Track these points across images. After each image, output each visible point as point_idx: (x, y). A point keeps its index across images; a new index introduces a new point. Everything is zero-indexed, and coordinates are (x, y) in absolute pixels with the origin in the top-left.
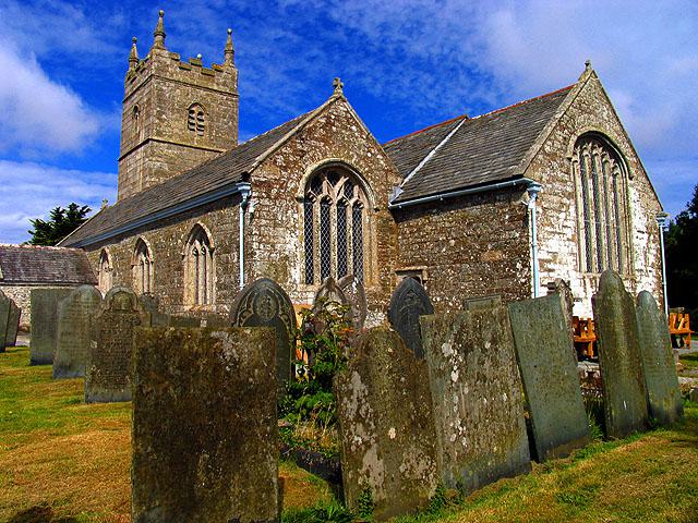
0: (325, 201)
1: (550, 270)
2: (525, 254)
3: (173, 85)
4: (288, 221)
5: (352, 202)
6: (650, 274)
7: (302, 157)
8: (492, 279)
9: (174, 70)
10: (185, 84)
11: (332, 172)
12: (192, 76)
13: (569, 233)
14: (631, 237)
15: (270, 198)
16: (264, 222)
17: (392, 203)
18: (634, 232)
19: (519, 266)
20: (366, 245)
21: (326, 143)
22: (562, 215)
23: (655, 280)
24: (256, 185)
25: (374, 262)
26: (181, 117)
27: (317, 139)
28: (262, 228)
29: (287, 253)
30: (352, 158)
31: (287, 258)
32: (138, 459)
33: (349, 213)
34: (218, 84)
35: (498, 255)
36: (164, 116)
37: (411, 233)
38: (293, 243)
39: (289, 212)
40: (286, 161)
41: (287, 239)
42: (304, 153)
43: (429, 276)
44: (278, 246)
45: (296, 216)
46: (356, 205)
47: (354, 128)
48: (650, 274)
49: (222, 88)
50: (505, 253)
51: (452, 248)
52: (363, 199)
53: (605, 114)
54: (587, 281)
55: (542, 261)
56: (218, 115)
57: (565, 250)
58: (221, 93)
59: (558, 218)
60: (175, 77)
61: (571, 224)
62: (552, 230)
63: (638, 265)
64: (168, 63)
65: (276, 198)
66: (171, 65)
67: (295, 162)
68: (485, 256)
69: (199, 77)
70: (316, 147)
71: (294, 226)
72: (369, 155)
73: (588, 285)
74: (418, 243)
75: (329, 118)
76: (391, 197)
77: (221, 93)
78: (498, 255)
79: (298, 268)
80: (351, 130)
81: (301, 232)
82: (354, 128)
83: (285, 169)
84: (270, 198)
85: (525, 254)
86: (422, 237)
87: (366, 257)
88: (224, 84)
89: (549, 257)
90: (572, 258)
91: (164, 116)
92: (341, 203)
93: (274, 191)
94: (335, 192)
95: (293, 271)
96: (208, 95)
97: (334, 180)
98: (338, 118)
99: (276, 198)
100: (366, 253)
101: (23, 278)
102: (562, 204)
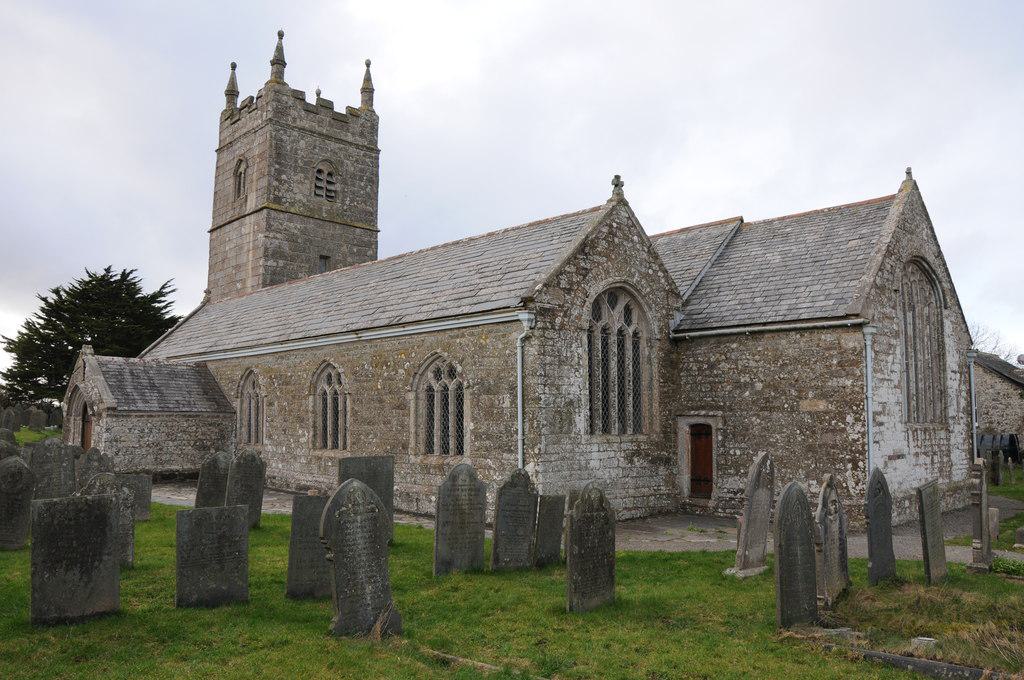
0: (604, 330)
1: (881, 424)
2: (858, 406)
3: (295, 133)
4: (572, 357)
5: (631, 330)
6: (962, 421)
7: (585, 277)
8: (814, 432)
10: (312, 132)
11: (612, 295)
12: (320, 122)
13: (895, 377)
14: (945, 378)
15: (554, 329)
17: (676, 331)
18: (949, 371)
19: (849, 419)
20: (644, 383)
21: (608, 256)
22: (890, 358)
23: (966, 428)
25: (656, 405)
26: (306, 178)
27: (600, 254)
29: (571, 396)
30: (633, 276)
31: (571, 403)
33: (629, 345)
34: (353, 134)
35: (822, 405)
36: (284, 177)
37: (699, 369)
40: (571, 283)
43: (725, 423)
45: (580, 351)
46: (635, 334)
47: (635, 238)
48: (962, 421)
50: (831, 403)
51: (758, 393)
52: (642, 328)
53: (924, 233)
54: (910, 432)
55: (875, 414)
56: (353, 177)
57: (893, 399)
58: (357, 146)
59: (887, 362)
60: (299, 123)
61: (897, 367)
62: (882, 377)
63: (952, 412)
64: (290, 103)
65: (560, 329)
67: (579, 283)
68: (805, 405)
69: (331, 125)
70: (599, 264)
72: (650, 272)
73: (911, 439)
74: (710, 383)
76: (673, 324)
77: (357, 146)
78: (822, 405)
79: (582, 415)
80: (632, 241)
81: (584, 371)
82: (635, 238)
84: (554, 329)
85: (858, 406)
86: (717, 376)
87: (645, 399)
89: (880, 409)
90: (898, 408)
91: (284, 177)
92: (620, 332)
93: (558, 320)
95: (577, 419)
96: (341, 149)
97: (613, 304)
99: (560, 329)
100: (645, 393)
101: (141, 405)
102: (890, 346)
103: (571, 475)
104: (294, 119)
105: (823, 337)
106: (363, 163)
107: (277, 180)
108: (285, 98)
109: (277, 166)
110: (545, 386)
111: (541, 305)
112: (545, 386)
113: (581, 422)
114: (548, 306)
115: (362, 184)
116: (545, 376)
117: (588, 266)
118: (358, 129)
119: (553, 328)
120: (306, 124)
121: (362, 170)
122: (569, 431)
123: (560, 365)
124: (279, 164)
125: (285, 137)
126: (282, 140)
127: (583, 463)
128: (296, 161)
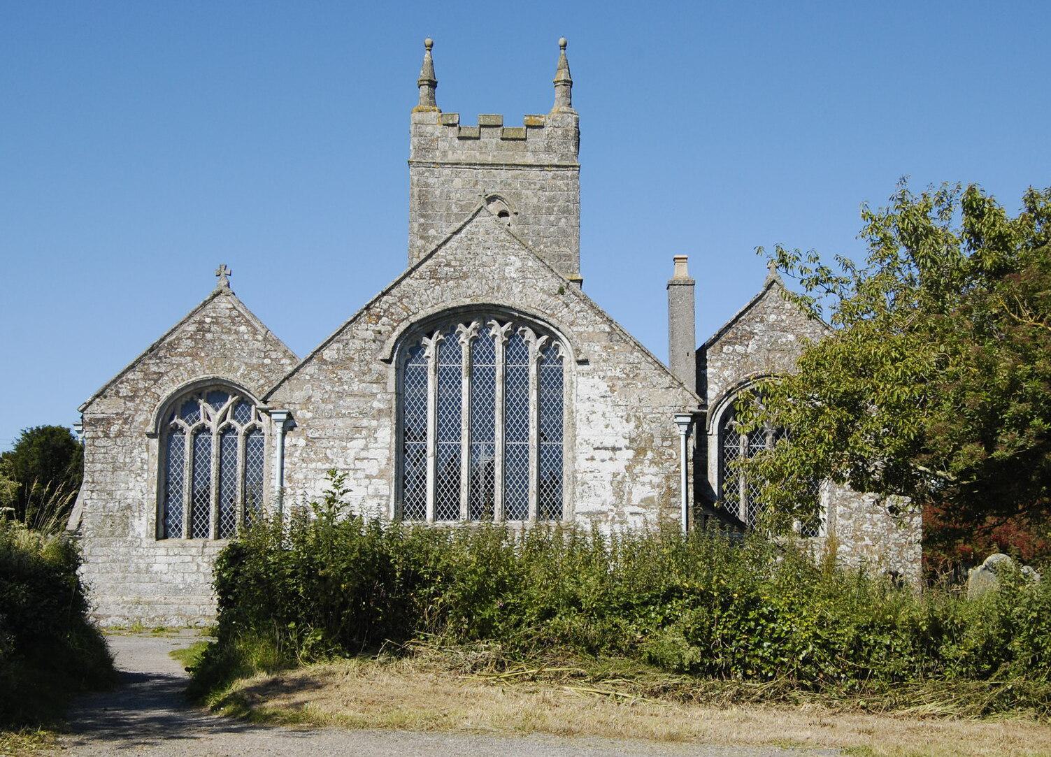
4: (133, 461)
9: (452, 148)
15: (109, 437)
16: (99, 466)
24: (90, 424)
27: (181, 355)
28: (97, 474)
29: (129, 501)
31: (129, 507)
32: (196, 708)
34: (535, 152)
36: (432, 232)
38: (138, 488)
39: (136, 451)
41: (131, 485)
42: (161, 375)
44: (118, 495)
47: (243, 328)
49: (545, 159)
56: (537, 210)
60: (451, 158)
64: (438, 133)
66: (444, 137)
67: (147, 389)
69: (499, 148)
70: (179, 365)
71: (142, 469)
75: (202, 323)
79: (144, 519)
80: (237, 333)
83: (132, 398)
84: (109, 437)
88: (548, 149)
93: (114, 429)
94: (212, 416)
95: (136, 522)
96: (516, 177)
98: (216, 321)
103: (125, 578)
104: (444, 153)
105: (942, 348)
106: (553, 188)
107: (422, 238)
108: (429, 129)
109: (422, 220)
110: (92, 492)
111: (92, 416)
112: (92, 492)
113: (144, 524)
114: (101, 416)
115: (552, 218)
116: (93, 482)
117: (163, 370)
118: (542, 144)
119: (107, 436)
120: (462, 156)
121: (550, 200)
122: (124, 534)
123: (115, 470)
124: (422, 216)
125: (432, 180)
126: (427, 185)
127: (143, 566)
128: (449, 209)
